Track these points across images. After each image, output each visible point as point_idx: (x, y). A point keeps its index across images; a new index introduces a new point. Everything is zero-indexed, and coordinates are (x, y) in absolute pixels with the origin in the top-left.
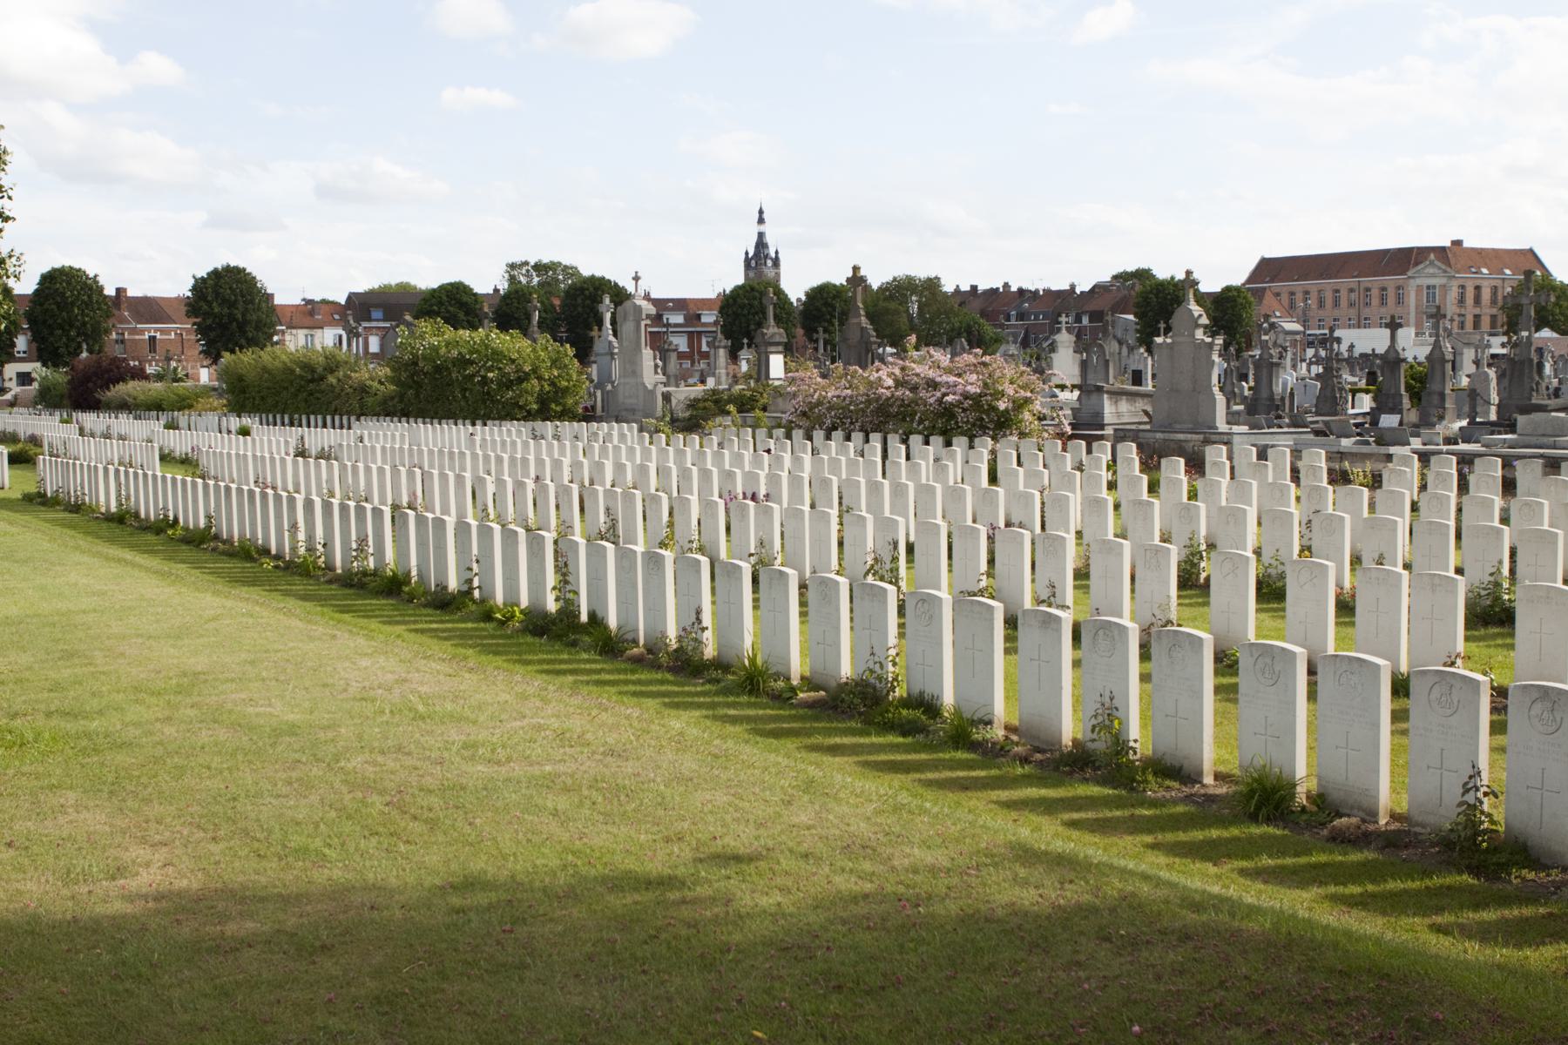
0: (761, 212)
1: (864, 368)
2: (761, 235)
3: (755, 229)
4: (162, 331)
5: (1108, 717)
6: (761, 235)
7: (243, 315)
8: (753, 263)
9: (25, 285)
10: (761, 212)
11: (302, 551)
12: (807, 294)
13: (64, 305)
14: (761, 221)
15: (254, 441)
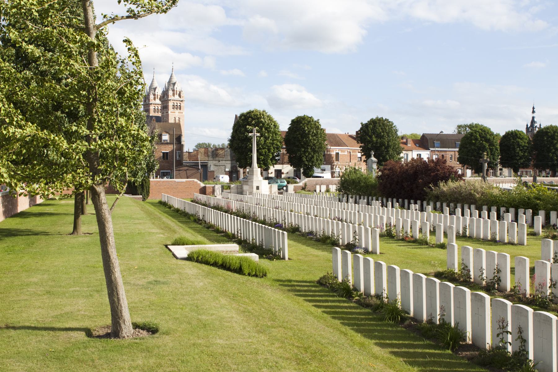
0: (533, 108)
1: (478, 170)
2: (533, 118)
3: (530, 115)
4: (342, 151)
5: (465, 268)
6: (533, 118)
7: (388, 142)
8: (530, 130)
9: (284, 126)
10: (533, 108)
11: (331, 233)
12: (183, 145)
13: (305, 135)
14: (533, 112)
15: (372, 208)
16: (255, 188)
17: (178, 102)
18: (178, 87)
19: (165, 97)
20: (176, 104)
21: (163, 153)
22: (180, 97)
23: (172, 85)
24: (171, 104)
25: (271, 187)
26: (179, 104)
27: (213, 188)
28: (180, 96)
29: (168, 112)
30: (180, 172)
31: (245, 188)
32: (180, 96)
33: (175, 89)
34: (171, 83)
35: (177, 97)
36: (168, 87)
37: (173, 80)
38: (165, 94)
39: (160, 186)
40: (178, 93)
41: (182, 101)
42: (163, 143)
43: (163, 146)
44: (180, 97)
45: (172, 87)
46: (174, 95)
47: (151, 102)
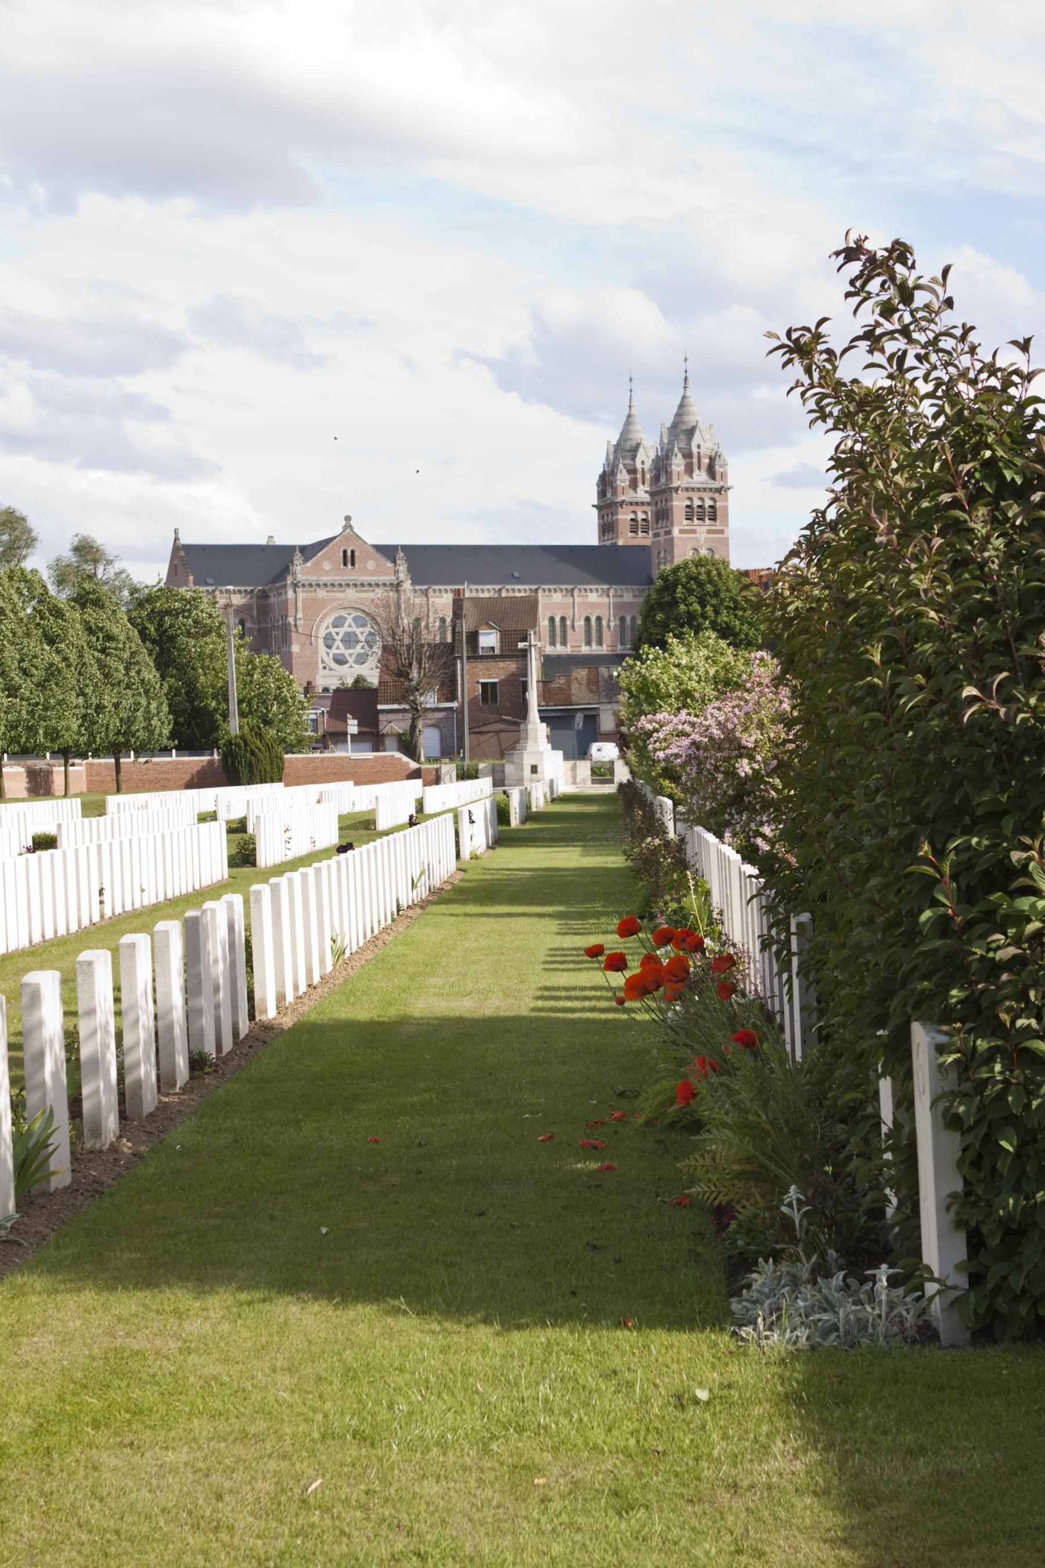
16: (527, 770)
17: (707, 496)
18: (703, 443)
19: (663, 480)
20: (697, 503)
21: (484, 685)
22: (713, 478)
23: (682, 436)
24: (679, 504)
25: (574, 768)
26: (708, 503)
27: (437, 770)
28: (711, 472)
29: (669, 533)
30: (482, 738)
31: (509, 769)
32: (711, 472)
33: (695, 450)
34: (681, 429)
35: (700, 477)
36: (671, 443)
37: (687, 418)
38: (661, 465)
39: (315, 769)
40: (706, 461)
41: (719, 490)
42: (482, 657)
43: (481, 666)
44: (713, 478)
45: (683, 445)
46: (689, 470)
47: (675, 484)
